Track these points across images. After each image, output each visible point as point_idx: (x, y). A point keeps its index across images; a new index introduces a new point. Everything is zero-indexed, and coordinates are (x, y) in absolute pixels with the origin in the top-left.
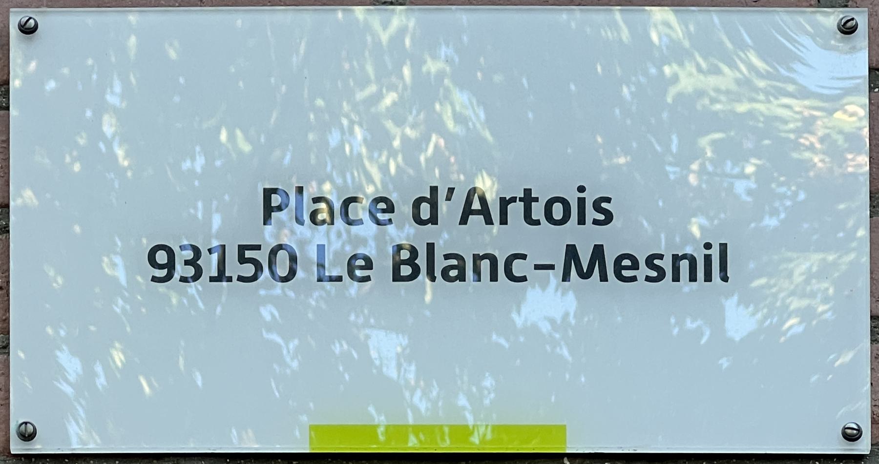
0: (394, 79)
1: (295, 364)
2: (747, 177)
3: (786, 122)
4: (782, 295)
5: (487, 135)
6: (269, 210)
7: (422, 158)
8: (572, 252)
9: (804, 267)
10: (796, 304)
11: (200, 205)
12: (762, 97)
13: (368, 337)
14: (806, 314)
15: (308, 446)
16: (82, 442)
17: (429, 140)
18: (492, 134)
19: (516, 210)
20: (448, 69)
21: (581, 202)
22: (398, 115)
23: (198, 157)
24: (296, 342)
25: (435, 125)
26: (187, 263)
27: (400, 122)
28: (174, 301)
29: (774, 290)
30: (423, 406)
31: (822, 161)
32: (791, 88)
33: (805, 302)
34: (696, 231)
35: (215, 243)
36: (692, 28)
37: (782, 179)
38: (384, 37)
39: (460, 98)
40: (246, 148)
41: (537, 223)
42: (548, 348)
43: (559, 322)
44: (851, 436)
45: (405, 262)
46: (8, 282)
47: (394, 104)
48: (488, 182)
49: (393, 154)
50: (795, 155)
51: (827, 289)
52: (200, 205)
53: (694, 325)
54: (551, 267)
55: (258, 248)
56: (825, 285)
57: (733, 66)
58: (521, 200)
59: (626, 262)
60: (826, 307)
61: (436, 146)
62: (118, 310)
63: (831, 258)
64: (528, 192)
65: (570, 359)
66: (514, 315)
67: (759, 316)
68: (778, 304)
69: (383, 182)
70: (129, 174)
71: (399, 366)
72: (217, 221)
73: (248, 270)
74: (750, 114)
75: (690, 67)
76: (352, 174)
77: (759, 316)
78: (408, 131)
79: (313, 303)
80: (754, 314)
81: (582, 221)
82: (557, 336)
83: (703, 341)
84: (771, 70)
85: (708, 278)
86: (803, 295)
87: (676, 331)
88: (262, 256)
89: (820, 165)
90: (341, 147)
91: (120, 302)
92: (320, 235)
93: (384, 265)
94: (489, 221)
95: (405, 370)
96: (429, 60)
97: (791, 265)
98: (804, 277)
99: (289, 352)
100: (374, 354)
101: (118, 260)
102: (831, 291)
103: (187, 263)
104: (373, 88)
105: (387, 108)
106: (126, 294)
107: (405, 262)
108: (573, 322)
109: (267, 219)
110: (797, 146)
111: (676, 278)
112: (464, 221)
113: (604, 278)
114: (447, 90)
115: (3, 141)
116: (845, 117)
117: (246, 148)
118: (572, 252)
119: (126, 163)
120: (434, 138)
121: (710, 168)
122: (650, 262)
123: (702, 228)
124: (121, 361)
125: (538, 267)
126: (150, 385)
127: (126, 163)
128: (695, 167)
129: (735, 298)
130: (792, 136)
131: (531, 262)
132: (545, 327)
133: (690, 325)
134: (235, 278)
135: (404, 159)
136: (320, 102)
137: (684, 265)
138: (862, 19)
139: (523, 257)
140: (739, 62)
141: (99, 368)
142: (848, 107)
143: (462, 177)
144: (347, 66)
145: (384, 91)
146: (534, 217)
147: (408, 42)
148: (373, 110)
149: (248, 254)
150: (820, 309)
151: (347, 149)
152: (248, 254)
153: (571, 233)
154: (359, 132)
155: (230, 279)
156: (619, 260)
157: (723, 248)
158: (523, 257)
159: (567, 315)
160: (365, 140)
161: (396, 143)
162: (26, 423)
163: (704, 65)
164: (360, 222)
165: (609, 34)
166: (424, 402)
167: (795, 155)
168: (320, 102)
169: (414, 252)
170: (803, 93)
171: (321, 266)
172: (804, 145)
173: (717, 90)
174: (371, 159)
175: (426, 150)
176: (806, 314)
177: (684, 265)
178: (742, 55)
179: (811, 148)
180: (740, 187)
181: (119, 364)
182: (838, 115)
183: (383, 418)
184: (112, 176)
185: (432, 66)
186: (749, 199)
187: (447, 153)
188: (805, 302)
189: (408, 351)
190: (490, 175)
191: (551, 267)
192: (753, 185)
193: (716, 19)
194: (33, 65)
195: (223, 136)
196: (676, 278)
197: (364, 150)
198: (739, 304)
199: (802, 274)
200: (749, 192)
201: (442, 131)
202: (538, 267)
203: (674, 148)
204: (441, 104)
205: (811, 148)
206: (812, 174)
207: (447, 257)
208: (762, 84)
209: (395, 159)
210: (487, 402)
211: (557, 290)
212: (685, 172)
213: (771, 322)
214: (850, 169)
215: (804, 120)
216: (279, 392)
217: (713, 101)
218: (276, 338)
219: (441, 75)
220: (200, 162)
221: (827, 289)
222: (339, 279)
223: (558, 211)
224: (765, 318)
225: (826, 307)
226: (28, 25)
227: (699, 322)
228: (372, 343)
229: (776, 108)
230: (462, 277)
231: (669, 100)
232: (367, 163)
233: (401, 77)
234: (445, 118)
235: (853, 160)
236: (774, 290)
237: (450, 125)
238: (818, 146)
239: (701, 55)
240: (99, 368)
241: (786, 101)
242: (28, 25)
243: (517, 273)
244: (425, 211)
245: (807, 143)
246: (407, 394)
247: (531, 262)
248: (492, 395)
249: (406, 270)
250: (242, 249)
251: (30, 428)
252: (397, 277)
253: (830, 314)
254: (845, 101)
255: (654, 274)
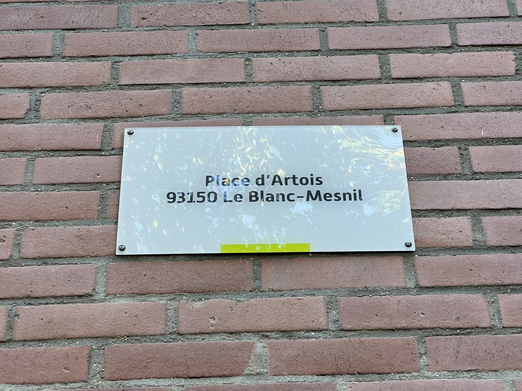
0: (250, 144)
1: (217, 225)
2: (368, 170)
3: (379, 155)
4: (382, 203)
5: (281, 159)
6: (208, 182)
7: (260, 165)
8: (309, 193)
9: (389, 195)
10: (387, 205)
11: (185, 179)
12: (370, 148)
13: (242, 217)
14: (392, 208)
15: (220, 251)
16: (142, 251)
17: (262, 160)
18: (282, 158)
19: (290, 181)
20: (268, 141)
21: (312, 179)
22: (251, 153)
23: (185, 166)
24: (217, 218)
25: (264, 156)
26: (180, 197)
27: (252, 155)
28: (176, 207)
29: (380, 201)
30: (261, 237)
31: (392, 165)
32: (379, 146)
33: (390, 205)
34: (352, 185)
35: (190, 191)
36: (346, 130)
37: (379, 170)
38: (247, 133)
39: (272, 149)
40: (202, 163)
41: (298, 184)
42: (304, 219)
43: (307, 211)
44: (408, 245)
45: (253, 196)
46: (119, 204)
47: (250, 150)
48: (282, 172)
49: (250, 164)
50: (382, 164)
51: (398, 201)
52: (185, 179)
53: (353, 212)
54: (302, 197)
55: (204, 193)
56: (397, 200)
57: (360, 140)
58: (292, 178)
59: (328, 195)
60: (398, 206)
61: (264, 162)
62: (156, 210)
63: (398, 192)
64: (294, 176)
65: (311, 222)
66: (292, 209)
67: (375, 209)
68: (381, 205)
69: (247, 172)
70: (162, 171)
71: (253, 225)
72: (191, 184)
73: (201, 199)
74: (367, 153)
75: (346, 140)
76: (237, 171)
77: (375, 209)
78: (255, 158)
79: (223, 207)
80: (373, 208)
81: (312, 184)
82: (307, 216)
83: (357, 217)
84: (372, 141)
85: (355, 199)
86: (390, 203)
87: (347, 214)
88: (205, 195)
89: (392, 166)
90: (233, 162)
91: (157, 208)
92: (226, 189)
93: (246, 197)
94: (281, 184)
95: (255, 227)
96: (261, 139)
97: (385, 194)
98: (389, 198)
99: (214, 221)
100: (244, 222)
101: (157, 196)
102: (399, 201)
103: (180, 197)
104: (243, 146)
105: (248, 152)
106: (159, 205)
107: (253, 196)
108: (312, 211)
109: (207, 185)
110: (383, 161)
111: (345, 199)
112: (273, 184)
113: (320, 200)
114: (268, 147)
115: (120, 164)
116: (399, 153)
117: (202, 163)
118: (309, 193)
119: (161, 168)
120: (263, 160)
121: (355, 167)
122: (336, 195)
123: (354, 184)
124: (156, 225)
125: (298, 197)
126: (166, 232)
127: (161, 168)
128: (350, 167)
129: (367, 204)
130: (381, 159)
131: (296, 196)
132: (302, 213)
133: (352, 212)
134: (196, 202)
135: (254, 166)
136: (226, 150)
137: (347, 196)
138: (399, 128)
139: (293, 194)
140: (362, 139)
141: (149, 228)
142: (399, 151)
143: (273, 171)
144: (235, 140)
145: (247, 147)
146: (296, 183)
147: (254, 134)
148: (243, 152)
149: (201, 194)
150: (396, 206)
151: (235, 163)
152: (201, 194)
153: (309, 187)
154: (239, 158)
155: (194, 202)
156: (325, 195)
157: (360, 191)
158: (293, 194)
159: (309, 210)
160: (241, 160)
161: (251, 161)
162: (122, 246)
163: (350, 140)
164: (239, 185)
165: (319, 131)
166: (261, 236)
167: (382, 164)
168: (226, 150)
169: (256, 193)
170: (384, 147)
171: (225, 196)
172: (385, 161)
173: (356, 147)
174: (243, 166)
175: (261, 163)
176: (392, 208)
177: (347, 196)
178: (363, 137)
179: (388, 162)
180: (365, 173)
181: (156, 226)
182: (396, 153)
183: (247, 241)
184: (156, 172)
185: (262, 140)
186: (369, 176)
187: (268, 164)
188: (390, 205)
189: (256, 221)
190: (282, 169)
191: (302, 197)
192: (369, 172)
193: (353, 128)
194: (132, 142)
195: (194, 160)
196: (345, 199)
197: (240, 163)
198: (368, 206)
199: (389, 196)
200: (369, 174)
201: (266, 158)
202: (298, 197)
203: (343, 162)
204: (266, 150)
205: (388, 162)
206: (389, 169)
207: (267, 195)
208: (370, 145)
209: (251, 166)
210: (283, 236)
211: (305, 202)
212: (347, 169)
213: (379, 211)
214: (401, 168)
215: (385, 154)
216: (211, 233)
217: (354, 149)
218: (210, 217)
219: (265, 143)
220: (186, 168)
221: (398, 201)
222: (231, 201)
223: (304, 181)
224: (377, 209)
225: (398, 206)
226: (130, 132)
227: (355, 211)
228: (243, 219)
229: (375, 151)
230: (273, 200)
231: (340, 149)
232: (241, 167)
233: (253, 143)
234: (267, 154)
235: (402, 165)
236: (380, 201)
237: (269, 156)
238: (390, 161)
239: (350, 137)
240: (149, 228)
241: (378, 149)
242: (130, 132)
243: (291, 199)
244: (260, 182)
245: (386, 161)
246: (255, 234)
247: (296, 196)
248: (285, 234)
249: (254, 199)
250: (198, 193)
251: (123, 247)
252: (251, 200)
253: (399, 208)
254: (398, 149)
255: (337, 199)
